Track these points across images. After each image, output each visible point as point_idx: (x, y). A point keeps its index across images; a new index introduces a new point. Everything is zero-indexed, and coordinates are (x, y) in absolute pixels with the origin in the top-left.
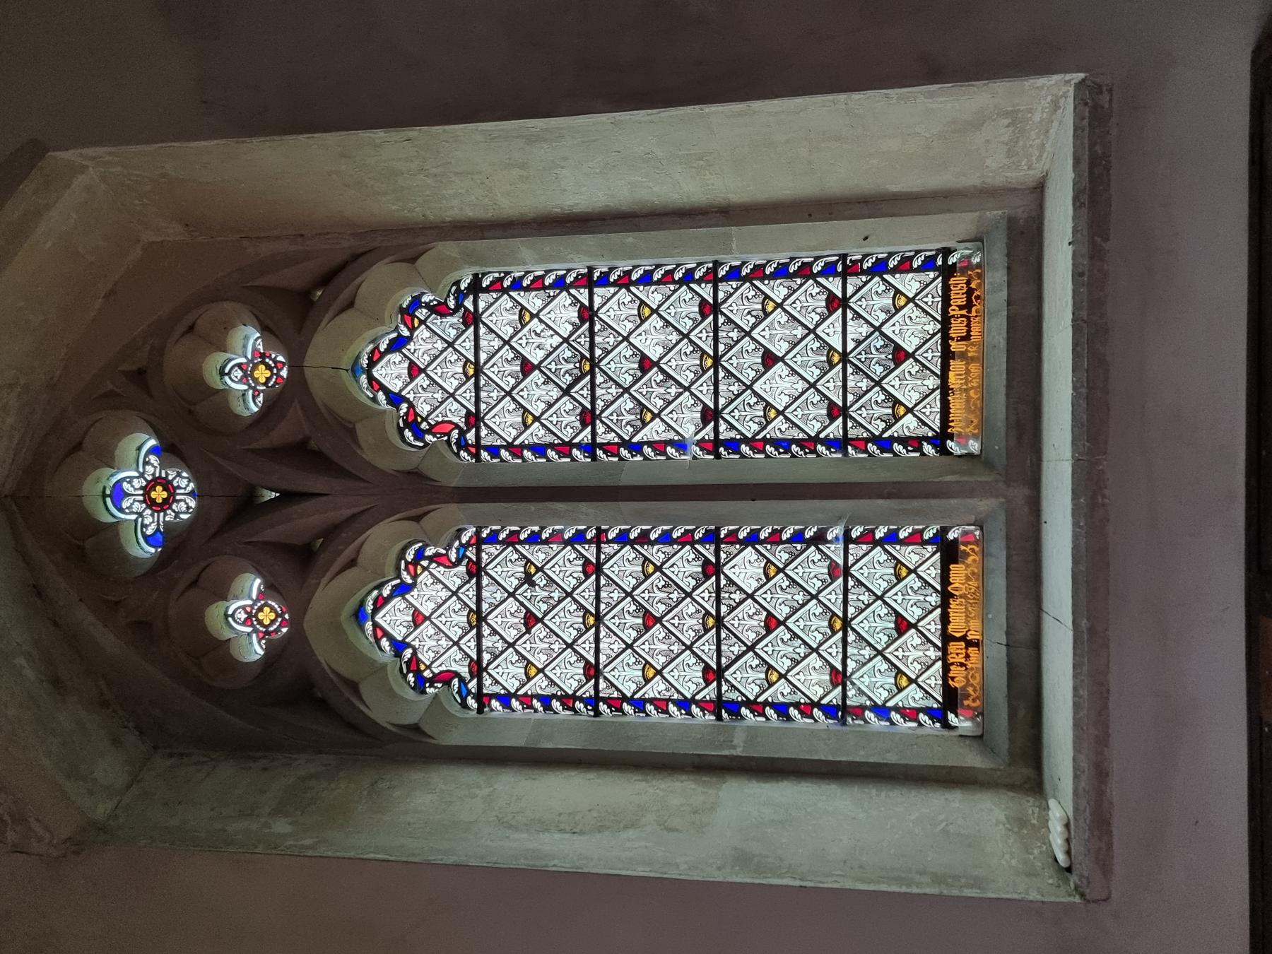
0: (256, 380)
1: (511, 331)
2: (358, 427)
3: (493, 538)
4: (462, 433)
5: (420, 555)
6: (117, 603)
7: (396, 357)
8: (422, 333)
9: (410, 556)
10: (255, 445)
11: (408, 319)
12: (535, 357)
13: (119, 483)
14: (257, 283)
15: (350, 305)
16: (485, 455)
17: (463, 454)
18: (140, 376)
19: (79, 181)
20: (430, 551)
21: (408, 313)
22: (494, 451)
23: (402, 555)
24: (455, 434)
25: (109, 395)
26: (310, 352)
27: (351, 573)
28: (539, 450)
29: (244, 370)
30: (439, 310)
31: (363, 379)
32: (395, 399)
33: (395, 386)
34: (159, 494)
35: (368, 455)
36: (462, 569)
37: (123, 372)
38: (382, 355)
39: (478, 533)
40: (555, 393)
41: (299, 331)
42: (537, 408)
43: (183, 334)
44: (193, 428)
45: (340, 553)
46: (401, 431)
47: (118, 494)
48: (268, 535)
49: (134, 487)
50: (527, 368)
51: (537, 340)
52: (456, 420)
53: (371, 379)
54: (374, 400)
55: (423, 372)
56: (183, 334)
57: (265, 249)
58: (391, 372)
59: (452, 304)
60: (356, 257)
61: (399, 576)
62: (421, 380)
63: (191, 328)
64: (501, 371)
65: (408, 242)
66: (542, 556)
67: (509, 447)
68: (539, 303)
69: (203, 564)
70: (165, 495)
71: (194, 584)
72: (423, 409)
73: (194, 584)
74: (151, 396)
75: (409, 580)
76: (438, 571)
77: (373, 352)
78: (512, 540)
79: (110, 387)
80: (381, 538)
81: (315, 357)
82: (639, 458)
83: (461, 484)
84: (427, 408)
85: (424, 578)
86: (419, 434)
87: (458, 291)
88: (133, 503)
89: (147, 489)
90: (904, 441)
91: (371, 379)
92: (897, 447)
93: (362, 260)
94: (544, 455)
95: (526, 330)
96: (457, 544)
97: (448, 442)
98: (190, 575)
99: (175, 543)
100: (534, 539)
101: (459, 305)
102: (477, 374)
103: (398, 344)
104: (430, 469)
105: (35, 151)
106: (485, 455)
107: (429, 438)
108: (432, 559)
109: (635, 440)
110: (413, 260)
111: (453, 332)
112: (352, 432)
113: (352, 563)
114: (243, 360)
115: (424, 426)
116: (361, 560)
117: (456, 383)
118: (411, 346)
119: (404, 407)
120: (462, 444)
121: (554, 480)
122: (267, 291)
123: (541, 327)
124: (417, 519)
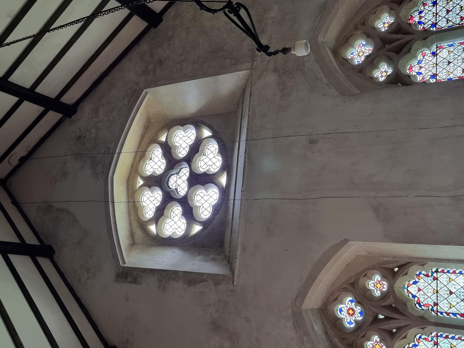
0: (377, 288)
1: (447, 283)
2: (407, 303)
3: (441, 336)
4: (432, 307)
5: (420, 337)
6: (344, 338)
7: (414, 286)
8: (421, 281)
9: (418, 337)
10: (381, 305)
11: (418, 277)
12: (453, 291)
13: (341, 308)
14: (384, 266)
15: (406, 274)
16: (439, 314)
17: (433, 312)
18: (352, 284)
19: (353, 247)
20: (423, 337)
21: (418, 276)
22: (442, 313)
23: (415, 337)
24: (430, 307)
25: (345, 288)
26: (396, 284)
27: (404, 340)
28: (455, 314)
29: (376, 285)
30: (427, 276)
31: (406, 290)
32: (414, 296)
33: (414, 293)
34: (351, 312)
35: (410, 311)
36: (432, 343)
37: (349, 284)
38: (411, 285)
39: (437, 334)
40: (459, 300)
41: (393, 279)
42: (454, 304)
43: (364, 276)
44: (363, 298)
45: (402, 334)
46: (415, 304)
47: (341, 311)
48: (383, 327)
49: (345, 310)
50: (451, 293)
51: (454, 286)
52: (431, 304)
53: (408, 290)
54: (409, 296)
55: (421, 290)
56: (364, 276)
57: (385, 259)
58: (413, 289)
59: (430, 274)
60: (408, 263)
61: (414, 342)
62: (421, 292)
63: (366, 275)
64: (443, 292)
65: (422, 262)
66: (456, 343)
67: (446, 313)
68: (455, 277)
69: (366, 332)
70: (352, 312)
71: (364, 336)
72: (422, 300)
73: (364, 336)
74: (355, 289)
75: (417, 344)
76: (426, 342)
77: (408, 284)
78: (447, 337)
79: (345, 286)
80: (411, 332)
81: (397, 285)
82: (442, 316)
83: (435, 321)
84: (423, 300)
85: (421, 343)
86: (420, 306)
87: (432, 271)
88: (345, 313)
89: (348, 310)
90: (453, 314)
91: (408, 290)
92: (451, 315)
93: (410, 264)
94: (442, 314)
95: (451, 283)
96: (431, 336)
97: (429, 309)
98: (362, 335)
99: (359, 326)
100: (453, 338)
101: (432, 275)
102: (437, 292)
103: (415, 283)
104: (426, 316)
105: (346, 241)
106: (439, 314)
107: (423, 307)
108: (423, 339)
109: (448, 312)
110: (423, 265)
111: (430, 282)
112: (406, 304)
113: (405, 337)
114: (374, 282)
115: (422, 304)
116: (407, 337)
117: (431, 294)
118: (419, 284)
119: (416, 299)
120: (432, 310)
121: (444, 322)
122: (384, 268)
123: (455, 283)
124: (423, 329)
